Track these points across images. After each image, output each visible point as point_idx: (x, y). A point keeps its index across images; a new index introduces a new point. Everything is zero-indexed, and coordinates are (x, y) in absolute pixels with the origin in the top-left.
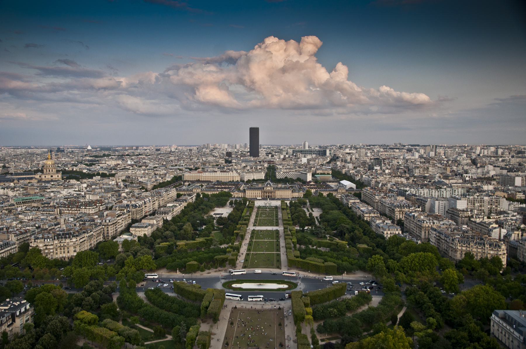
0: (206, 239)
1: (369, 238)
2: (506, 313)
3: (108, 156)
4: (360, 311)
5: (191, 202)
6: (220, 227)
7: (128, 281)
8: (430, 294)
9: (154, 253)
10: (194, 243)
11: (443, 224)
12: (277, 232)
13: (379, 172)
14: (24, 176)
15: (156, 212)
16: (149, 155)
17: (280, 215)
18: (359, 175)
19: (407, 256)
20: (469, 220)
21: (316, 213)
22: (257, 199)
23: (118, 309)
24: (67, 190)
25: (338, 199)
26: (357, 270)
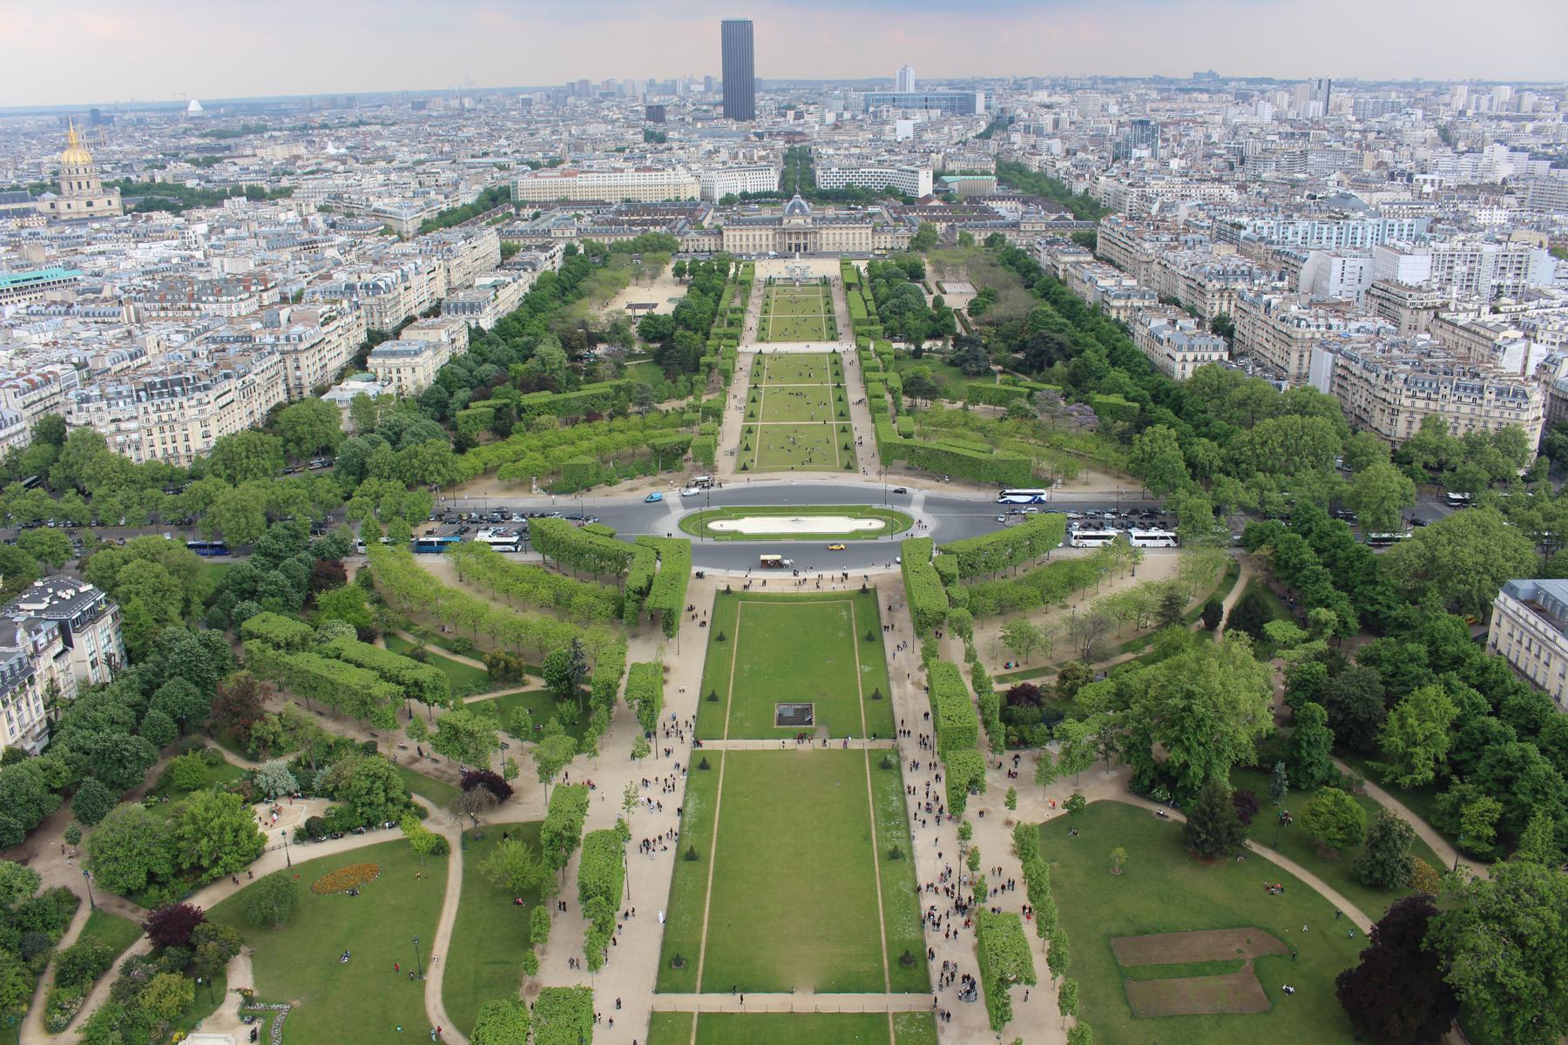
2: (1538, 588)
3: (260, 130)
5: (550, 268)
8: (1321, 538)
12: (836, 359)
13: (1147, 166)
15: (444, 303)
16: (393, 124)
17: (839, 307)
18: (1087, 176)
24: (147, 245)
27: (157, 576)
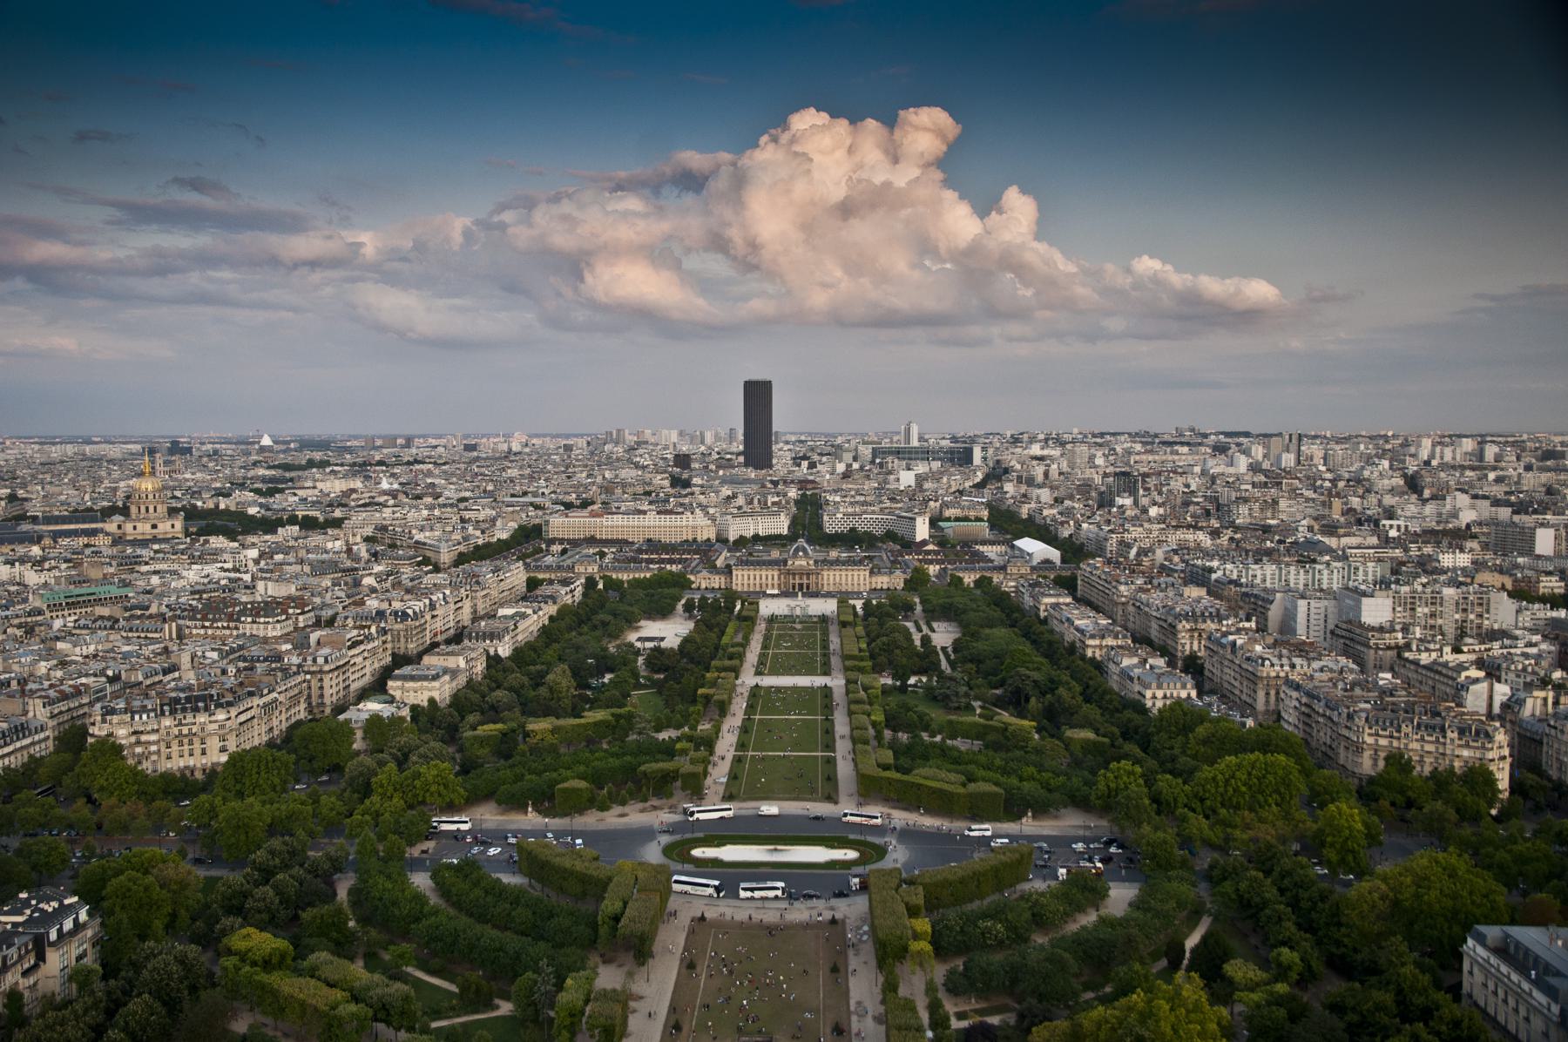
0: (613, 715)
1: (1099, 711)
2: (1507, 936)
3: (323, 464)
4: (1072, 927)
5: (570, 602)
6: (656, 676)
7: (382, 838)
8: (1283, 877)
9: (458, 756)
10: (578, 725)
11: (1321, 670)
12: (827, 691)
13: (1129, 513)
14: (72, 527)
15: (466, 632)
16: (444, 464)
17: (835, 642)
18: (1072, 523)
19: (1212, 764)
20: (1399, 656)
21: (943, 636)
22: (765, 595)
23: (351, 924)
24: (199, 567)
25: (1008, 594)
26: (1065, 807)
27: (146, 889)
